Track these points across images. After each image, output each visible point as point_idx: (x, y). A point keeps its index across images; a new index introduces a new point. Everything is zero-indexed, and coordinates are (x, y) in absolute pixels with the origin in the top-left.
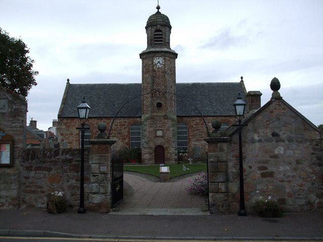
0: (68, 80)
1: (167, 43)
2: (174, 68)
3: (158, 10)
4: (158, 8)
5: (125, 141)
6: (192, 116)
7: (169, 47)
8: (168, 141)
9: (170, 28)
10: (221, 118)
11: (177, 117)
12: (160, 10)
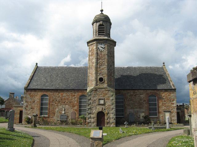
0: (37, 64)
1: (108, 34)
2: (114, 52)
3: (102, 12)
4: (102, 11)
5: (75, 108)
6: (127, 89)
7: (109, 35)
8: (104, 77)
9: (111, 24)
10: (150, 91)
11: (116, 90)
12: (103, 12)
